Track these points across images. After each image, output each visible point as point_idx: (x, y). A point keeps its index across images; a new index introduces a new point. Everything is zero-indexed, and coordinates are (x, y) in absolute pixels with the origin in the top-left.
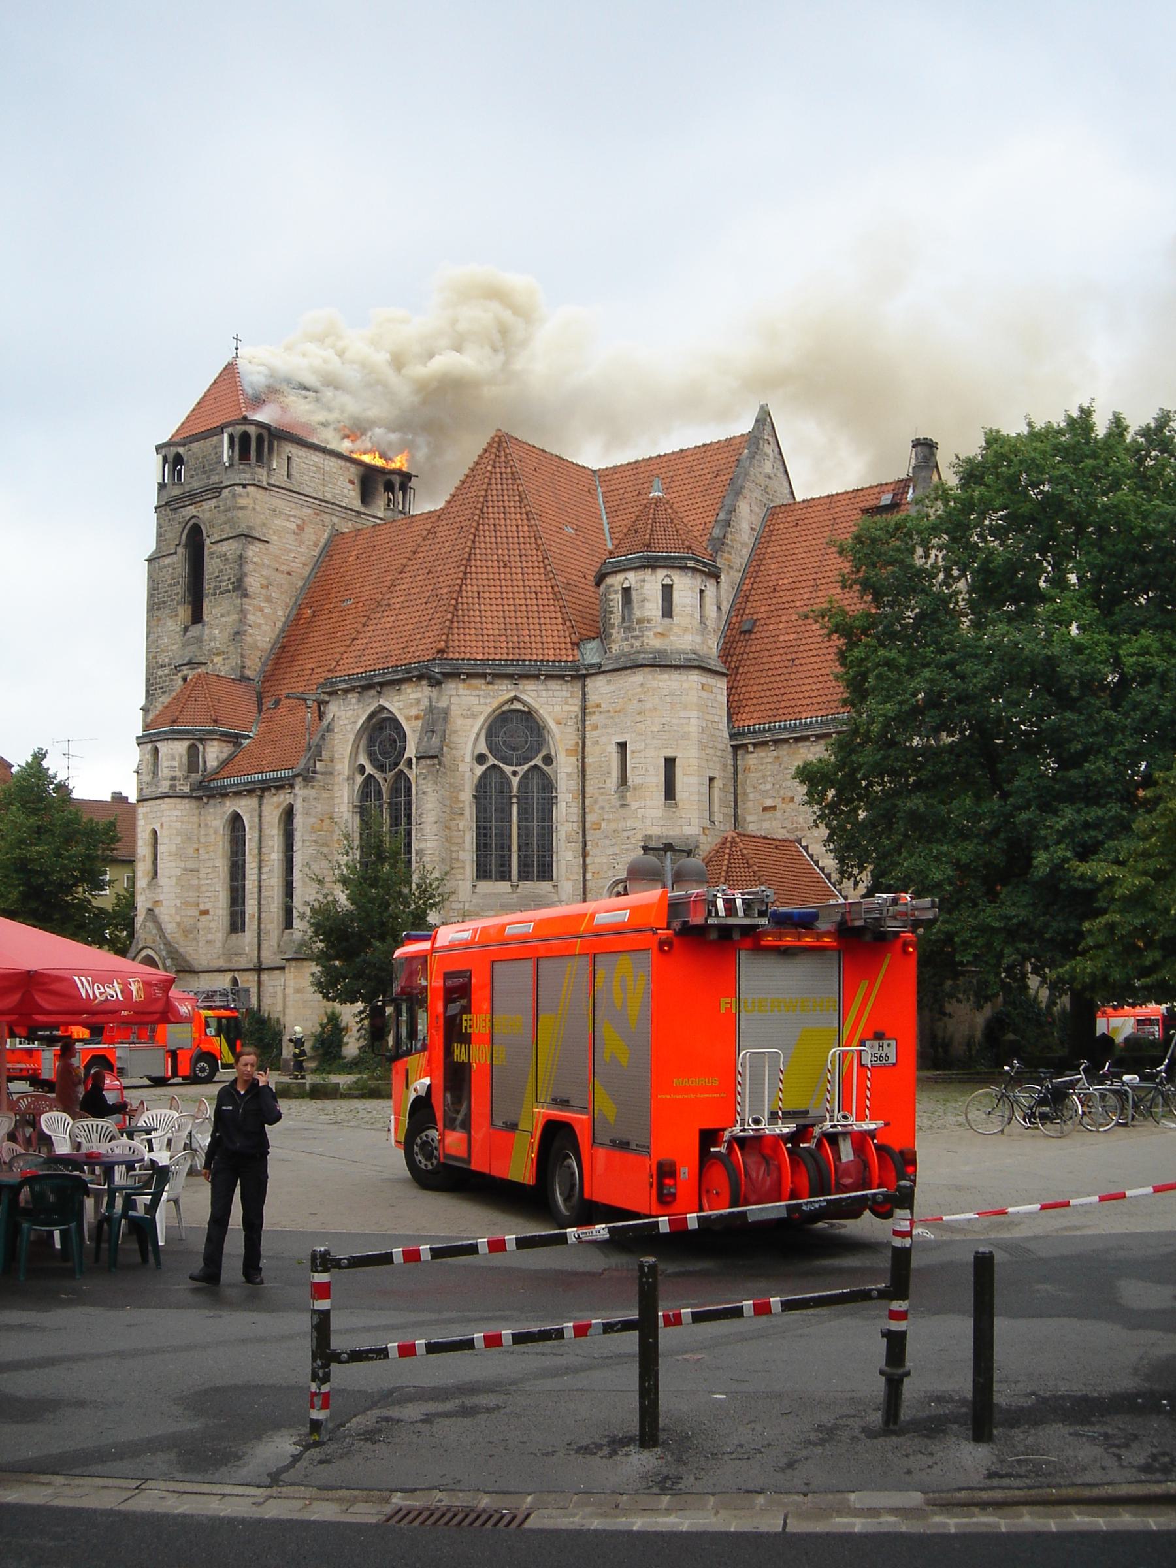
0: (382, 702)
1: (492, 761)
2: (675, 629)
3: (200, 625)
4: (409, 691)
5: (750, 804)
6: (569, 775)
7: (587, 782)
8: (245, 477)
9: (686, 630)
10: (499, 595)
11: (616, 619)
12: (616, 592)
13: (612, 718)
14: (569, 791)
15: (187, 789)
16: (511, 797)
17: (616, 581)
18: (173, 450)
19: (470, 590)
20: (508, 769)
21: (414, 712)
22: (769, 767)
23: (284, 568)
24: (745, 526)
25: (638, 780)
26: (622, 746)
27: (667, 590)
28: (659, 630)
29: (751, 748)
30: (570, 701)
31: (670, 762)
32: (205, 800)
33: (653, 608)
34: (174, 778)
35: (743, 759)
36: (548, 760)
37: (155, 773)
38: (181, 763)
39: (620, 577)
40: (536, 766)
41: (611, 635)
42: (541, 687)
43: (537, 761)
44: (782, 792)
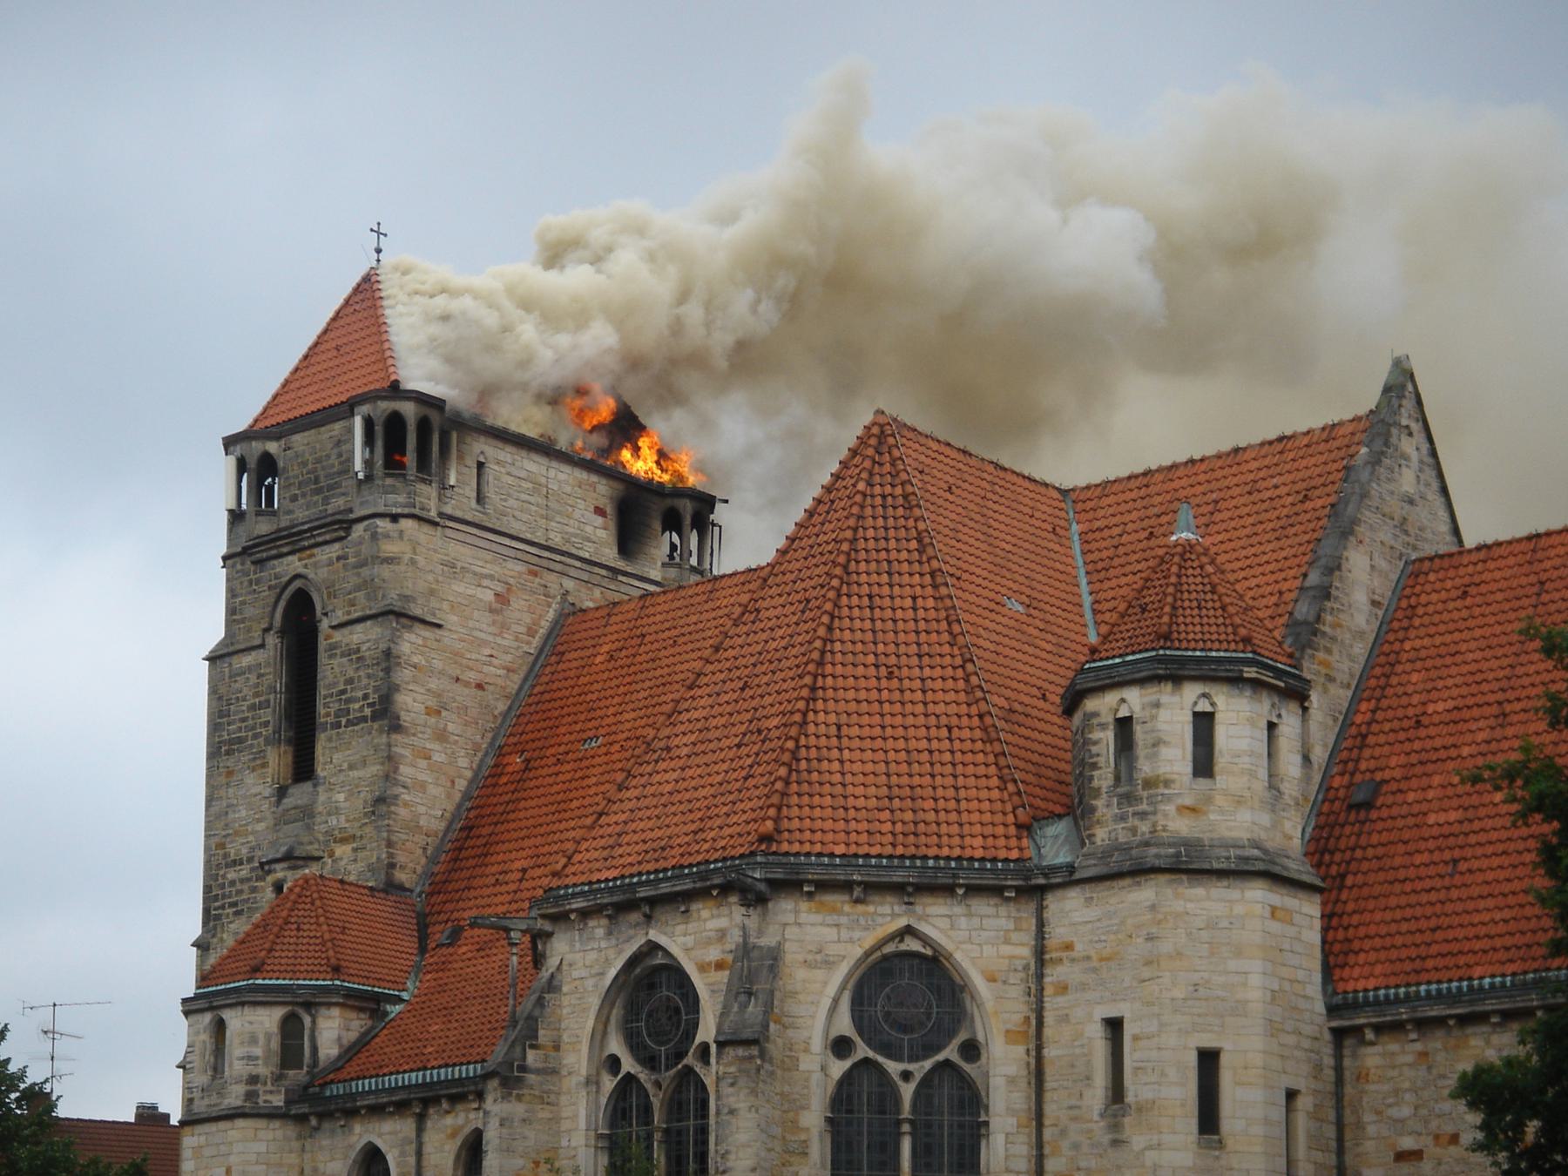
0: (654, 935)
1: (863, 1051)
2: (1220, 800)
3: (307, 786)
4: (705, 914)
5: (1369, 1146)
6: (1011, 1081)
7: (1048, 1096)
8: (396, 501)
9: (1239, 801)
10: (877, 731)
11: (1103, 778)
12: (1103, 726)
13: (1095, 970)
14: (1011, 1111)
15: (278, 1100)
16: (899, 1123)
17: (1103, 705)
18: (257, 447)
19: (824, 719)
20: (893, 1067)
21: (714, 954)
22: (1407, 1072)
23: (472, 676)
24: (1360, 598)
25: (1147, 1094)
26: (1114, 1026)
27: (1204, 723)
28: (1188, 801)
29: (1370, 1035)
30: (1015, 937)
31: (1209, 1060)
32: (314, 1122)
33: (1175, 759)
34: (253, 1079)
35: (1354, 1056)
36: (971, 1050)
37: (217, 1069)
38: (268, 1051)
39: (1111, 698)
40: (947, 1063)
41: (1093, 810)
42: (958, 910)
43: (950, 1053)
44: (1434, 1124)
